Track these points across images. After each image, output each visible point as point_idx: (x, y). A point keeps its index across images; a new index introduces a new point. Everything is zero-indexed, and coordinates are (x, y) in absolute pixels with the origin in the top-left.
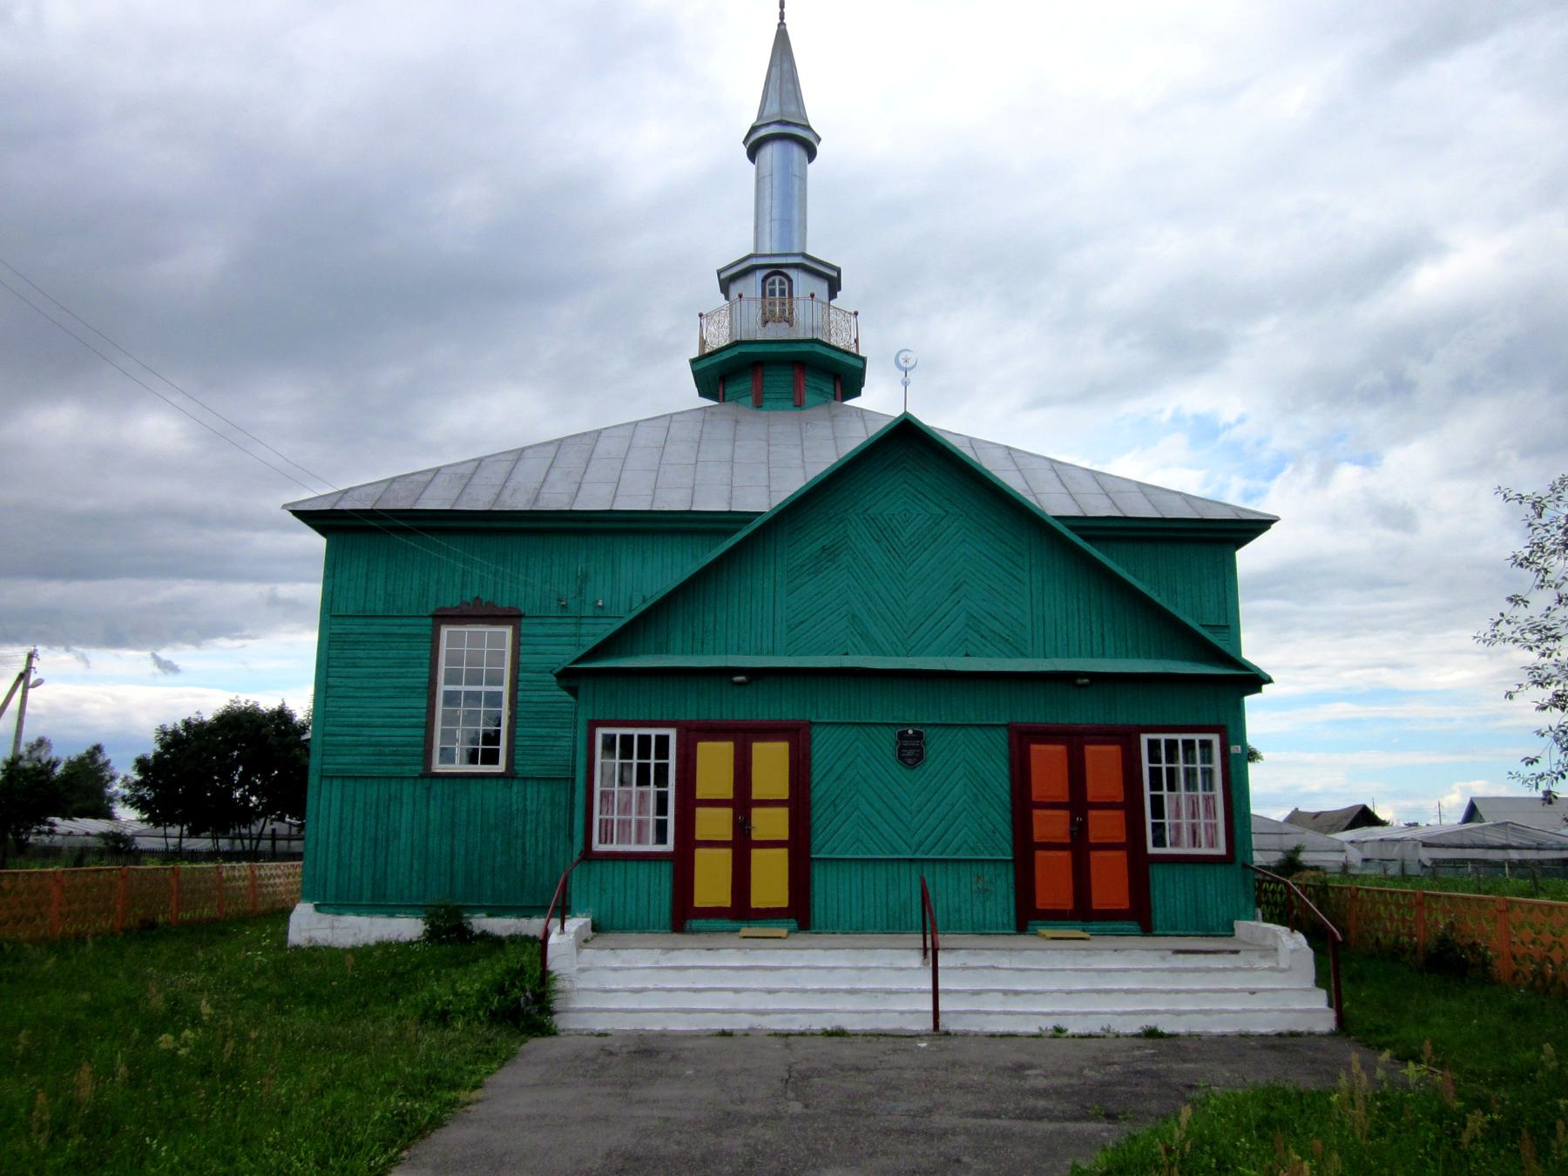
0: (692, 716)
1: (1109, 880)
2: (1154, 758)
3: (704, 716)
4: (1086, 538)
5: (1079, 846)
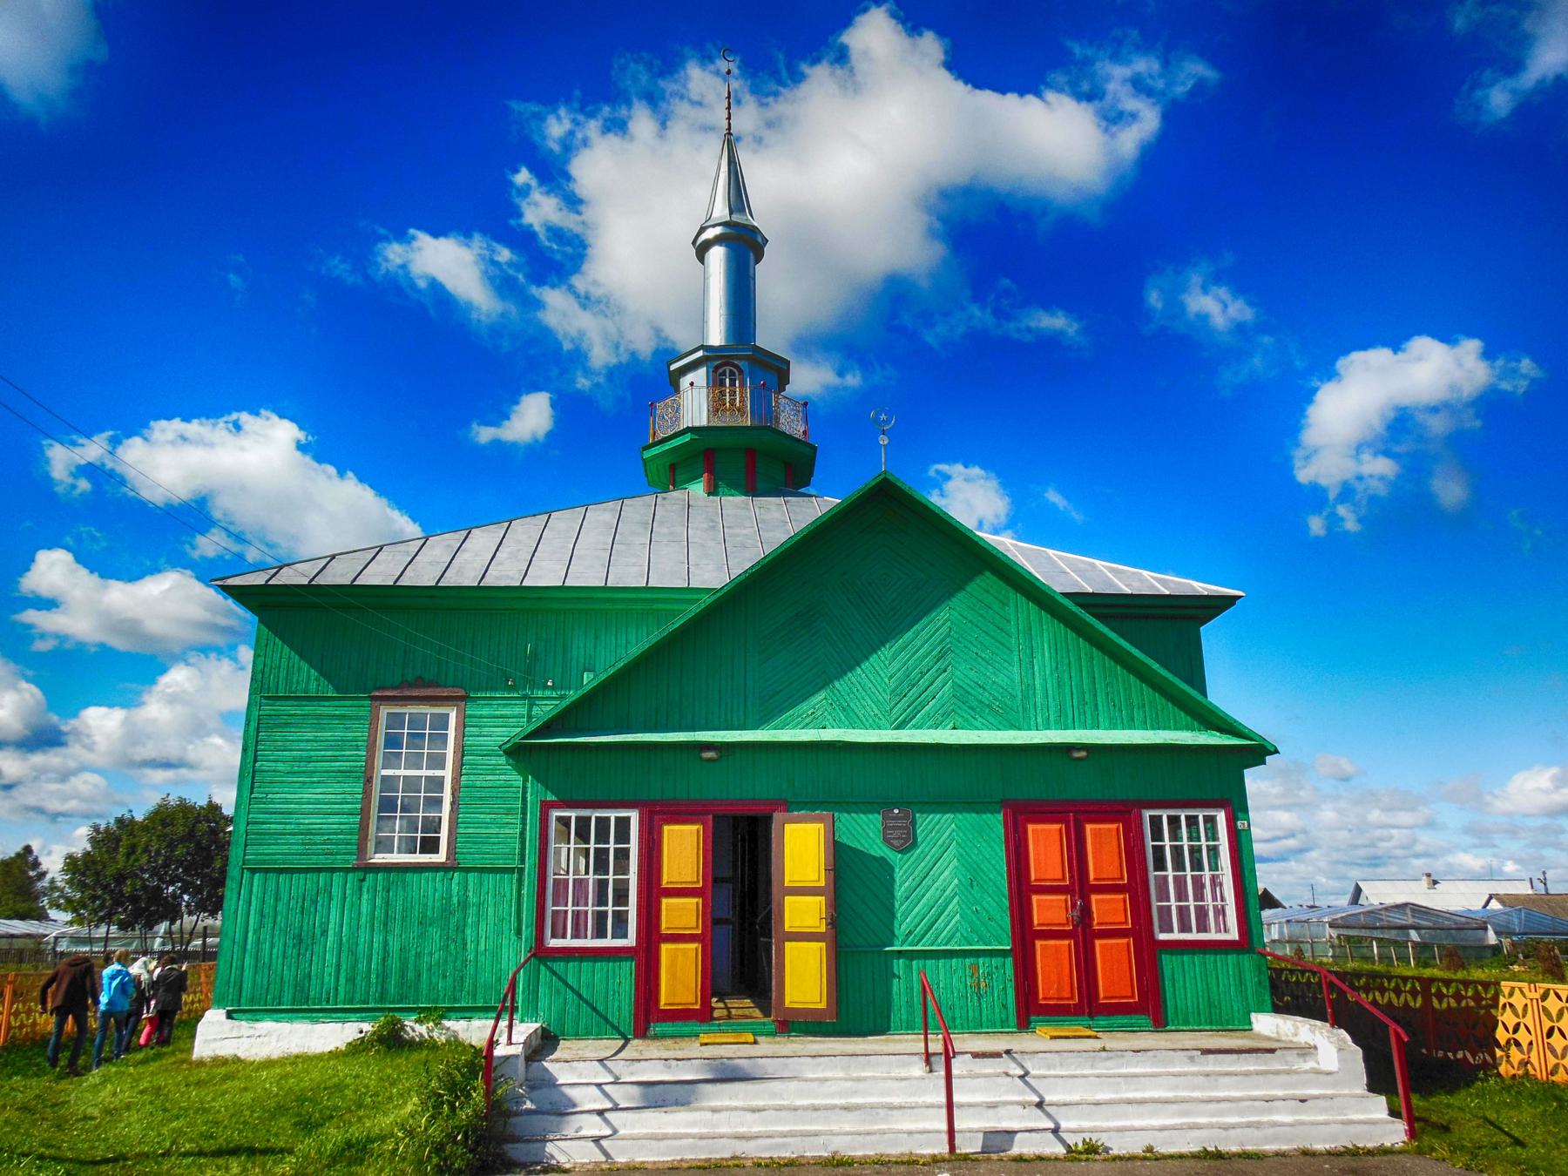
0: (655, 795)
1: (1114, 964)
2: (621, 919)
3: (669, 795)
4: (1097, 616)
5: (1083, 934)
